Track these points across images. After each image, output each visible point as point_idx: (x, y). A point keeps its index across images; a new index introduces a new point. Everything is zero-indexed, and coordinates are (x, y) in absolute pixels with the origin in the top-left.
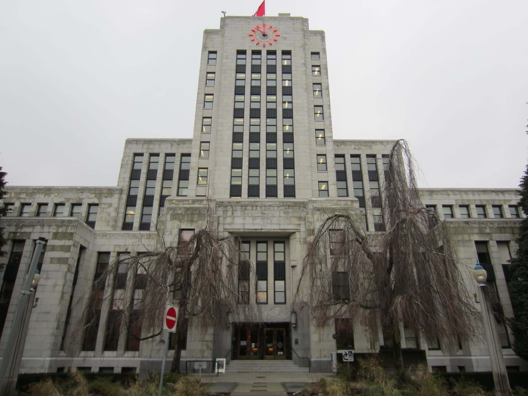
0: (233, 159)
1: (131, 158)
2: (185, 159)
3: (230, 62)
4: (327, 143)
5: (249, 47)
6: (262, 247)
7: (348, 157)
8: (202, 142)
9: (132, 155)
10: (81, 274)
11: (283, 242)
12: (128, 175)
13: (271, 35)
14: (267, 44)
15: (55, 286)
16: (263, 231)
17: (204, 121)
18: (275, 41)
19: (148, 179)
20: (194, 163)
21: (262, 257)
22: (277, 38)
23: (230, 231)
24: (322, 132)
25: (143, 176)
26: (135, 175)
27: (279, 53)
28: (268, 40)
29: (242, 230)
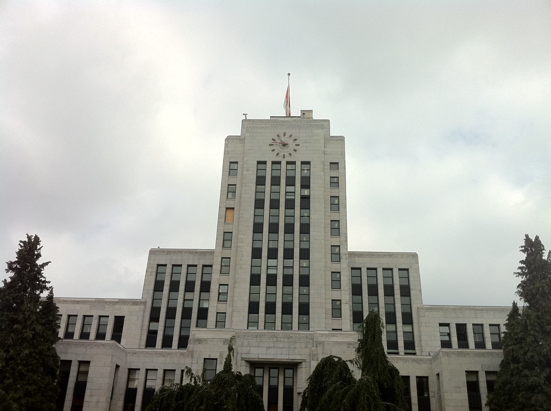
0: (256, 200)
1: (155, 270)
2: (206, 270)
3: (250, 175)
4: (341, 260)
5: (269, 158)
6: (274, 372)
7: (364, 271)
8: (222, 258)
9: (156, 266)
10: (116, 391)
11: (293, 369)
12: (152, 287)
13: (292, 145)
14: (287, 154)
15: (98, 402)
16: (275, 360)
17: (226, 238)
18: (295, 150)
19: (171, 290)
20: (216, 279)
21: (274, 382)
22: (296, 148)
23: (247, 360)
24: (336, 253)
25: (166, 288)
26: (158, 286)
27: (298, 164)
28: (288, 149)
29: (256, 360)
